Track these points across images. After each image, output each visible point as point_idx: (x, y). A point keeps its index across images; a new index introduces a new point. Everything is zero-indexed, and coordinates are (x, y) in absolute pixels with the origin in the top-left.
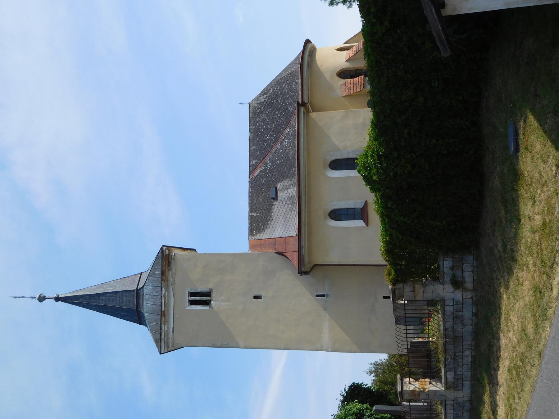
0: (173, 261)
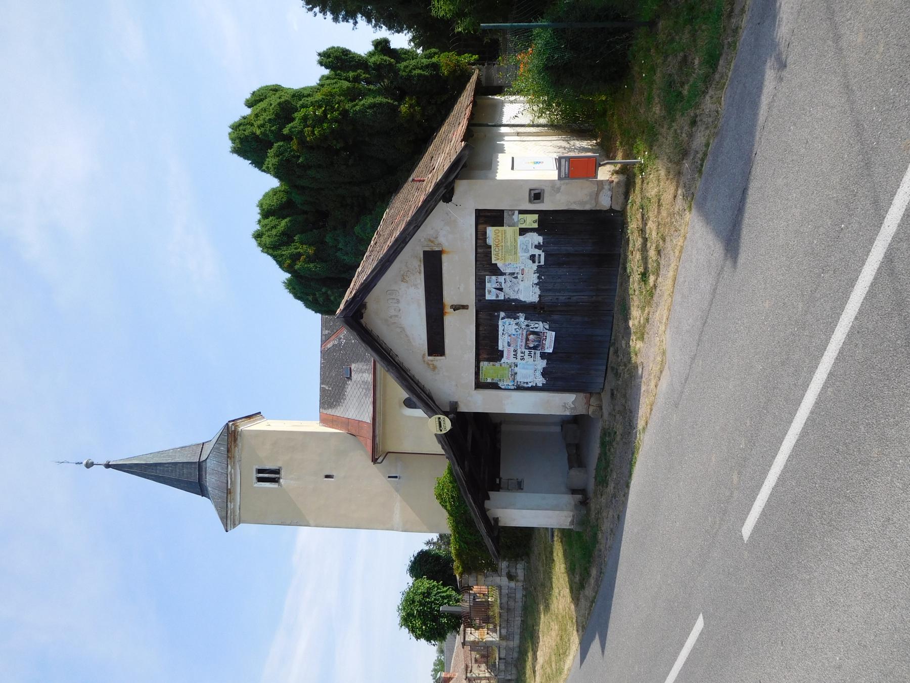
0: (239, 437)
